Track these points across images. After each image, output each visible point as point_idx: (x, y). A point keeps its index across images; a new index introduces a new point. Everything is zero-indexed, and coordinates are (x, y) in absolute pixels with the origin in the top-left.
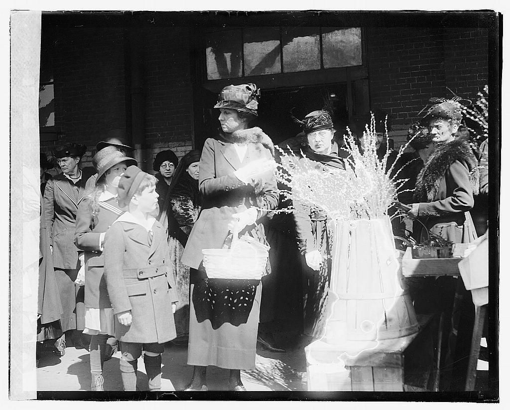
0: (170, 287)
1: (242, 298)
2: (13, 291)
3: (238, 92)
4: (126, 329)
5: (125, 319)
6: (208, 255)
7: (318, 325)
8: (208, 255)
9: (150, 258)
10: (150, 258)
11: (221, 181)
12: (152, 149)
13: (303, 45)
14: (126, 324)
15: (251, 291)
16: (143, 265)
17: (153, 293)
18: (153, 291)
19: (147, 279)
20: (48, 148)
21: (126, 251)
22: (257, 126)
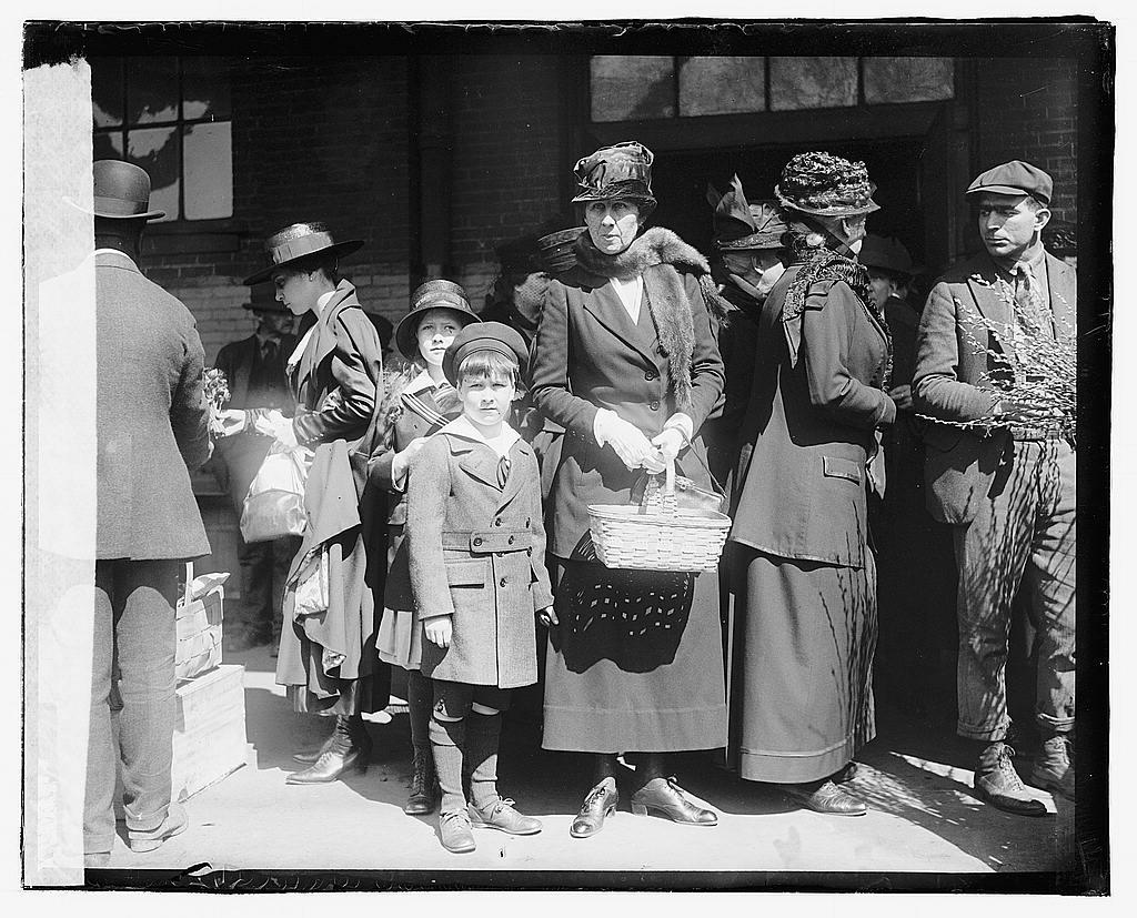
0: (534, 579)
1: (649, 611)
2: (28, 728)
3: (619, 160)
4: (435, 653)
5: (440, 632)
6: (610, 520)
7: (746, 692)
8: (610, 520)
9: (498, 513)
10: (498, 513)
11: (569, 422)
12: (465, 275)
13: (705, 69)
14: (440, 643)
15: (680, 590)
16: (484, 526)
17: (498, 585)
18: (498, 581)
19: (490, 554)
20: (216, 266)
21: (452, 494)
22: (695, 247)
